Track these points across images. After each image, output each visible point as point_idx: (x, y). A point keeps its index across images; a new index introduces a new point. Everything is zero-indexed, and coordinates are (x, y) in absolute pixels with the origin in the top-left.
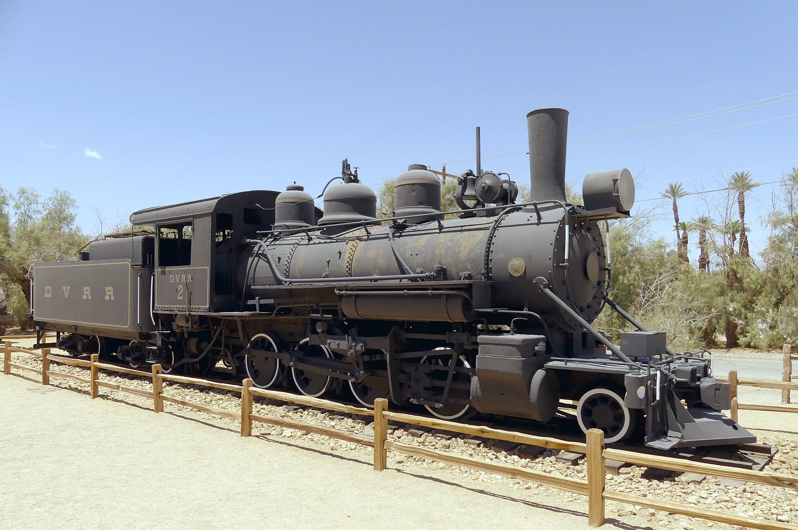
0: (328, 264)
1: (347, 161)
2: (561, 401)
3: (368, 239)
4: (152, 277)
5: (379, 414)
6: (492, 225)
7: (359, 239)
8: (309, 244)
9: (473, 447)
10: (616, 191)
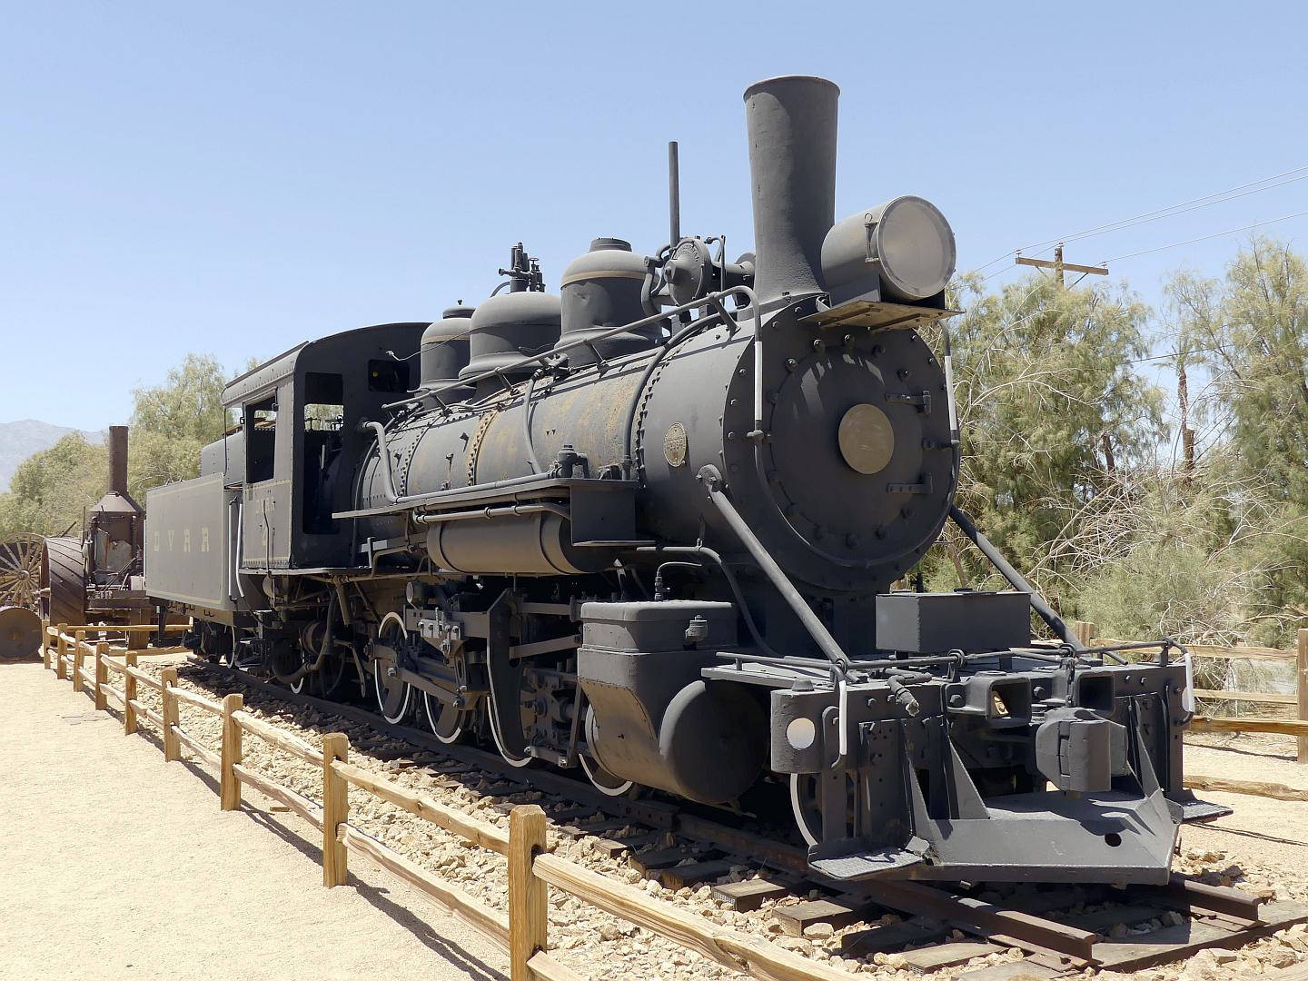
1: (521, 247)
7: (500, 407)
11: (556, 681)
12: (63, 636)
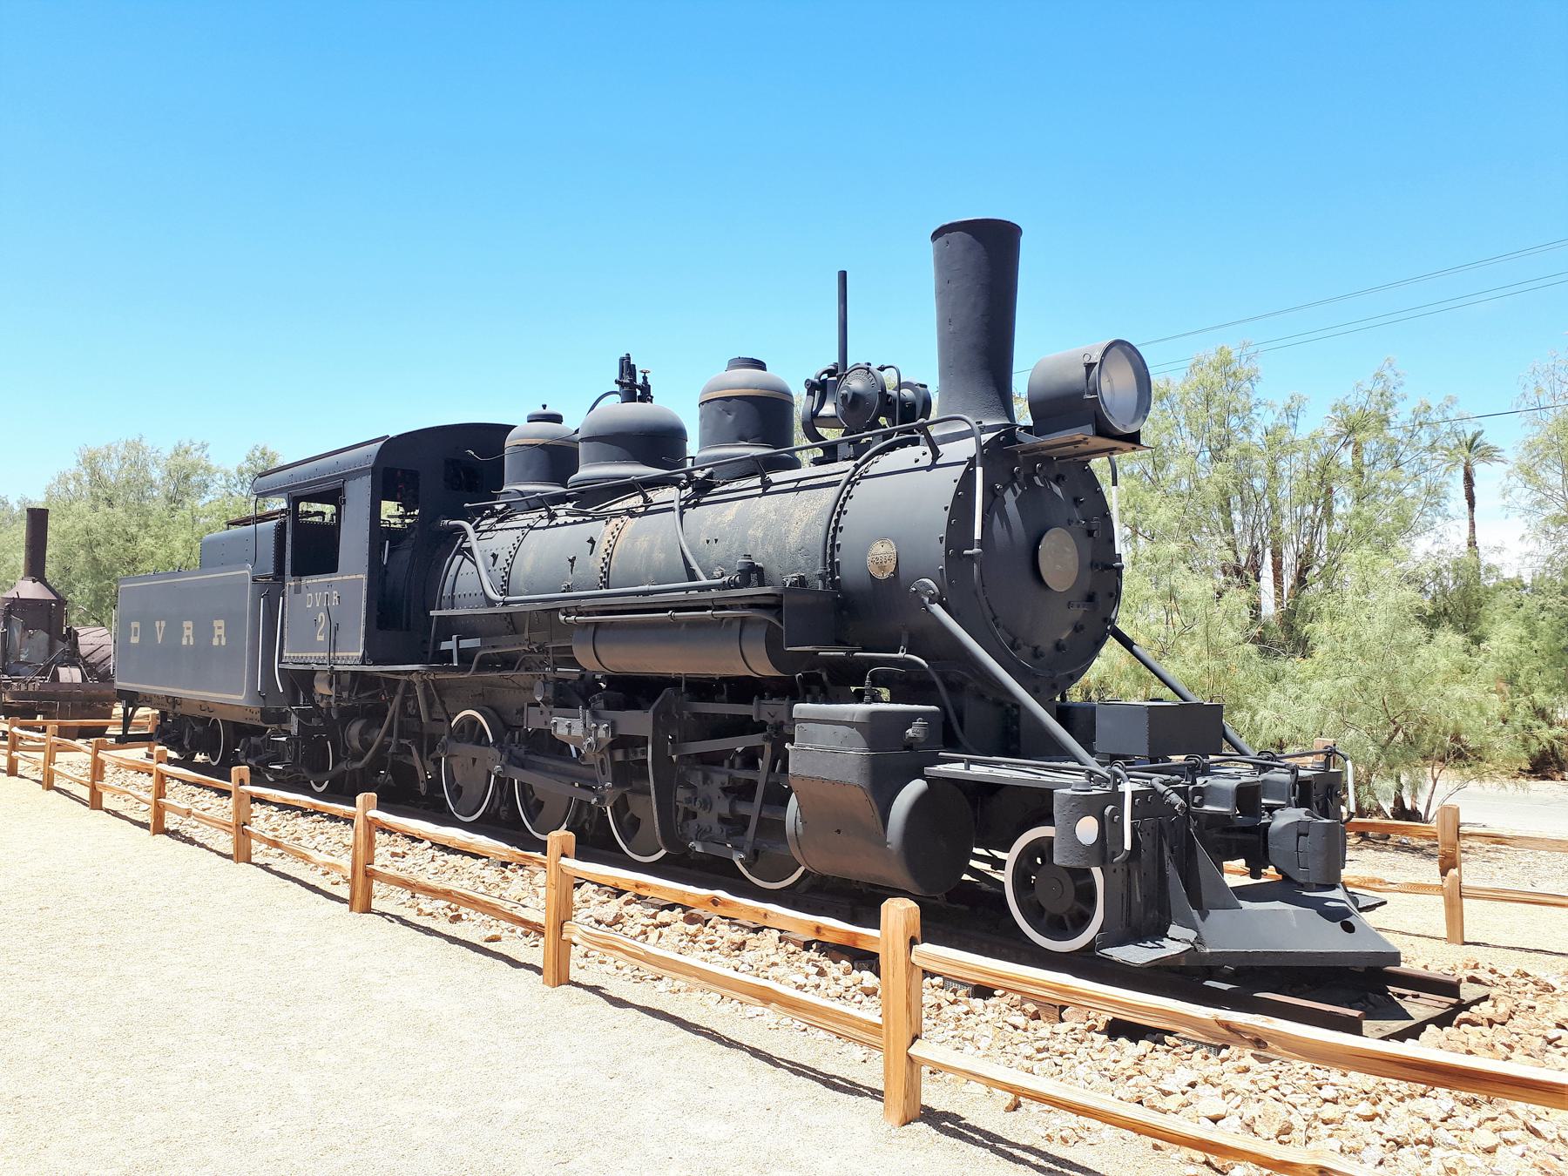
0: (572, 566)
1: (629, 358)
2: (977, 851)
3: (646, 513)
4: (281, 598)
5: (553, 863)
6: (845, 477)
7: (631, 513)
8: (548, 527)
9: (791, 948)
10: (1091, 388)
11: (725, 779)
12: (15, 730)
